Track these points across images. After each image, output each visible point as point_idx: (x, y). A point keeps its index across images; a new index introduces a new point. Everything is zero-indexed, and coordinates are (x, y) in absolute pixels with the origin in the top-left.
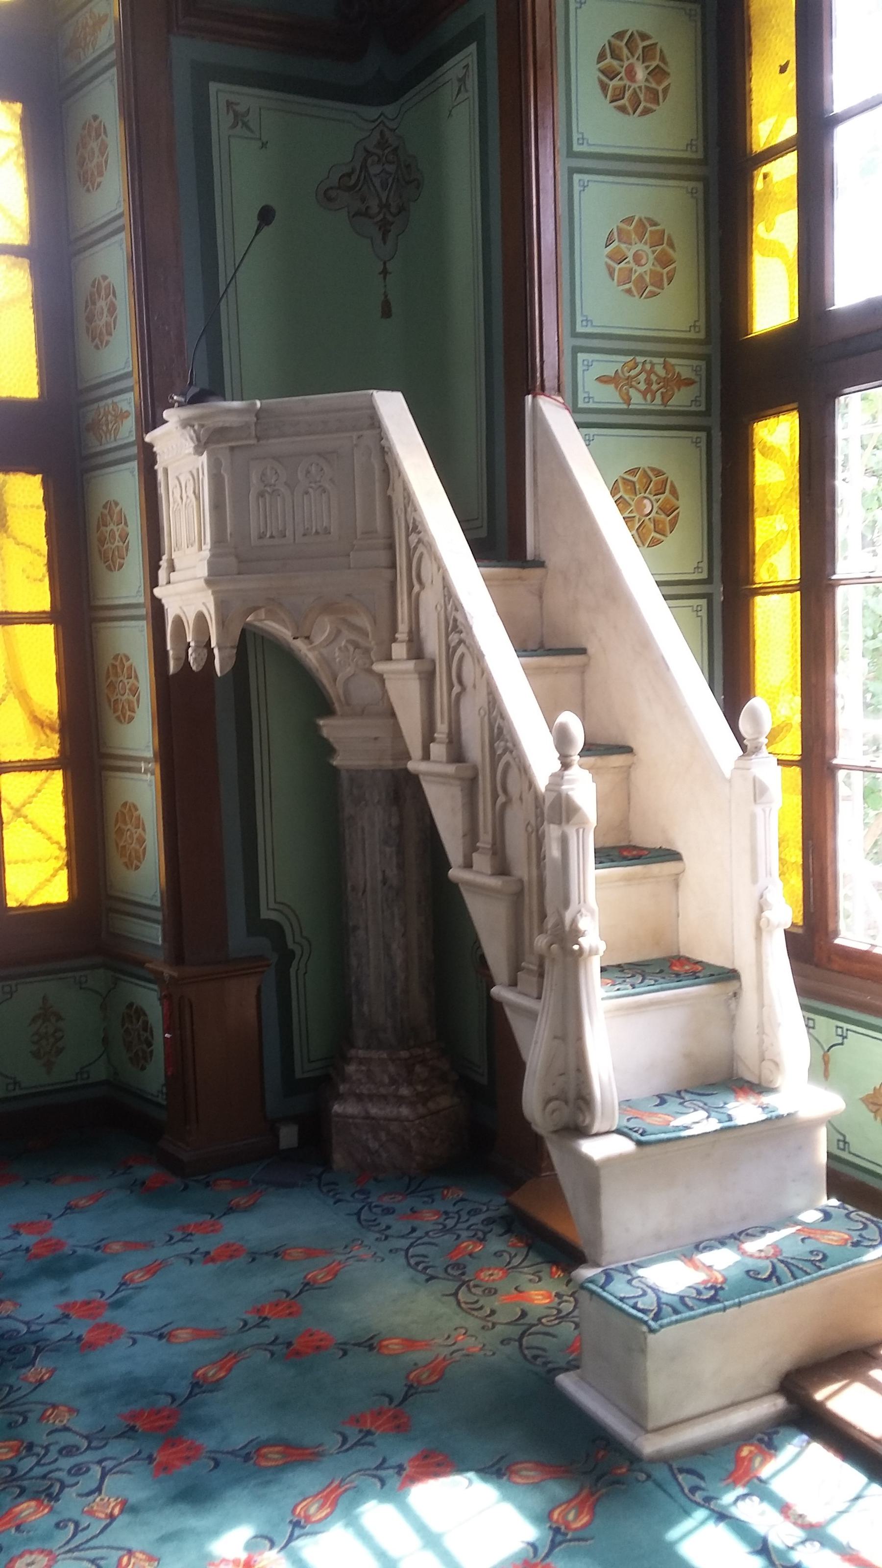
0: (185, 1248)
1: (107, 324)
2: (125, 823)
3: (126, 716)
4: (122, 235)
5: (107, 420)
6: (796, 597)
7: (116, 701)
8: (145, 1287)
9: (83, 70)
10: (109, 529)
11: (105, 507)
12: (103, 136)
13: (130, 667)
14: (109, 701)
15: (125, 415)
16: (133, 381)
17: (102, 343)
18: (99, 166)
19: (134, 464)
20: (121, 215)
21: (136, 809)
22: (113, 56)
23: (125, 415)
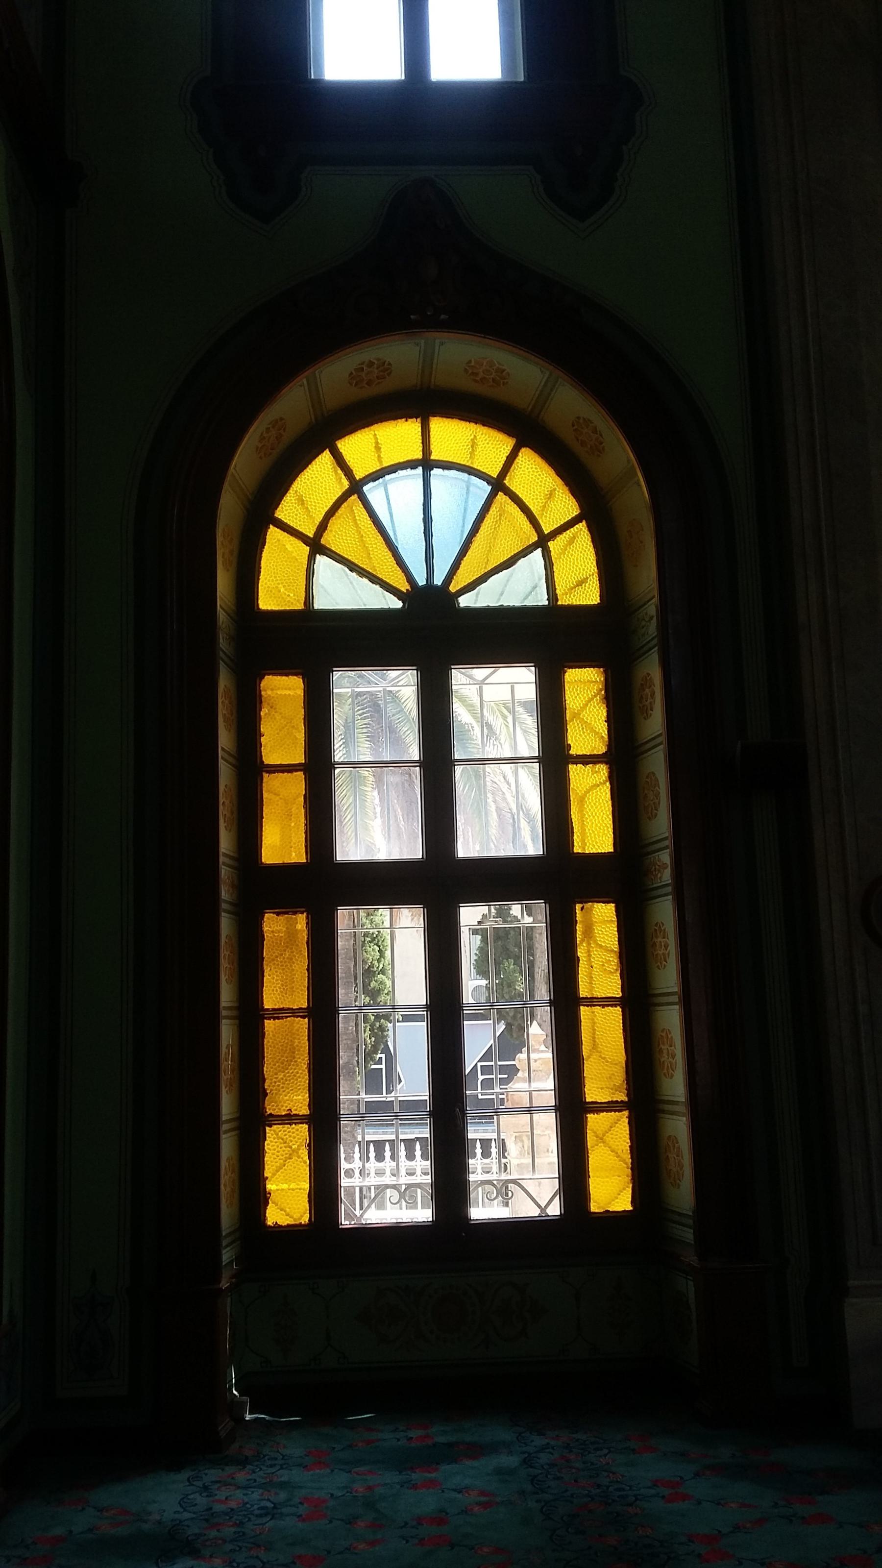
0: (472, 731)
1: (651, 703)
2: (663, 1044)
3: (646, 712)
4: (661, 747)
5: (655, 869)
6: (310, 532)
7: (657, 955)
8: (212, 1482)
9: (642, 647)
10: (645, 692)
11: (647, 777)
12: (653, 686)
13: (679, 1148)
14: (660, 1061)
15: (665, 866)
16: (663, 739)
17: (647, 715)
18: (651, 703)
19: (670, 897)
20: (661, 735)
21: (677, 1142)
22: (655, 641)
23: (665, 866)
